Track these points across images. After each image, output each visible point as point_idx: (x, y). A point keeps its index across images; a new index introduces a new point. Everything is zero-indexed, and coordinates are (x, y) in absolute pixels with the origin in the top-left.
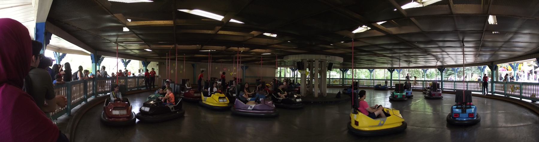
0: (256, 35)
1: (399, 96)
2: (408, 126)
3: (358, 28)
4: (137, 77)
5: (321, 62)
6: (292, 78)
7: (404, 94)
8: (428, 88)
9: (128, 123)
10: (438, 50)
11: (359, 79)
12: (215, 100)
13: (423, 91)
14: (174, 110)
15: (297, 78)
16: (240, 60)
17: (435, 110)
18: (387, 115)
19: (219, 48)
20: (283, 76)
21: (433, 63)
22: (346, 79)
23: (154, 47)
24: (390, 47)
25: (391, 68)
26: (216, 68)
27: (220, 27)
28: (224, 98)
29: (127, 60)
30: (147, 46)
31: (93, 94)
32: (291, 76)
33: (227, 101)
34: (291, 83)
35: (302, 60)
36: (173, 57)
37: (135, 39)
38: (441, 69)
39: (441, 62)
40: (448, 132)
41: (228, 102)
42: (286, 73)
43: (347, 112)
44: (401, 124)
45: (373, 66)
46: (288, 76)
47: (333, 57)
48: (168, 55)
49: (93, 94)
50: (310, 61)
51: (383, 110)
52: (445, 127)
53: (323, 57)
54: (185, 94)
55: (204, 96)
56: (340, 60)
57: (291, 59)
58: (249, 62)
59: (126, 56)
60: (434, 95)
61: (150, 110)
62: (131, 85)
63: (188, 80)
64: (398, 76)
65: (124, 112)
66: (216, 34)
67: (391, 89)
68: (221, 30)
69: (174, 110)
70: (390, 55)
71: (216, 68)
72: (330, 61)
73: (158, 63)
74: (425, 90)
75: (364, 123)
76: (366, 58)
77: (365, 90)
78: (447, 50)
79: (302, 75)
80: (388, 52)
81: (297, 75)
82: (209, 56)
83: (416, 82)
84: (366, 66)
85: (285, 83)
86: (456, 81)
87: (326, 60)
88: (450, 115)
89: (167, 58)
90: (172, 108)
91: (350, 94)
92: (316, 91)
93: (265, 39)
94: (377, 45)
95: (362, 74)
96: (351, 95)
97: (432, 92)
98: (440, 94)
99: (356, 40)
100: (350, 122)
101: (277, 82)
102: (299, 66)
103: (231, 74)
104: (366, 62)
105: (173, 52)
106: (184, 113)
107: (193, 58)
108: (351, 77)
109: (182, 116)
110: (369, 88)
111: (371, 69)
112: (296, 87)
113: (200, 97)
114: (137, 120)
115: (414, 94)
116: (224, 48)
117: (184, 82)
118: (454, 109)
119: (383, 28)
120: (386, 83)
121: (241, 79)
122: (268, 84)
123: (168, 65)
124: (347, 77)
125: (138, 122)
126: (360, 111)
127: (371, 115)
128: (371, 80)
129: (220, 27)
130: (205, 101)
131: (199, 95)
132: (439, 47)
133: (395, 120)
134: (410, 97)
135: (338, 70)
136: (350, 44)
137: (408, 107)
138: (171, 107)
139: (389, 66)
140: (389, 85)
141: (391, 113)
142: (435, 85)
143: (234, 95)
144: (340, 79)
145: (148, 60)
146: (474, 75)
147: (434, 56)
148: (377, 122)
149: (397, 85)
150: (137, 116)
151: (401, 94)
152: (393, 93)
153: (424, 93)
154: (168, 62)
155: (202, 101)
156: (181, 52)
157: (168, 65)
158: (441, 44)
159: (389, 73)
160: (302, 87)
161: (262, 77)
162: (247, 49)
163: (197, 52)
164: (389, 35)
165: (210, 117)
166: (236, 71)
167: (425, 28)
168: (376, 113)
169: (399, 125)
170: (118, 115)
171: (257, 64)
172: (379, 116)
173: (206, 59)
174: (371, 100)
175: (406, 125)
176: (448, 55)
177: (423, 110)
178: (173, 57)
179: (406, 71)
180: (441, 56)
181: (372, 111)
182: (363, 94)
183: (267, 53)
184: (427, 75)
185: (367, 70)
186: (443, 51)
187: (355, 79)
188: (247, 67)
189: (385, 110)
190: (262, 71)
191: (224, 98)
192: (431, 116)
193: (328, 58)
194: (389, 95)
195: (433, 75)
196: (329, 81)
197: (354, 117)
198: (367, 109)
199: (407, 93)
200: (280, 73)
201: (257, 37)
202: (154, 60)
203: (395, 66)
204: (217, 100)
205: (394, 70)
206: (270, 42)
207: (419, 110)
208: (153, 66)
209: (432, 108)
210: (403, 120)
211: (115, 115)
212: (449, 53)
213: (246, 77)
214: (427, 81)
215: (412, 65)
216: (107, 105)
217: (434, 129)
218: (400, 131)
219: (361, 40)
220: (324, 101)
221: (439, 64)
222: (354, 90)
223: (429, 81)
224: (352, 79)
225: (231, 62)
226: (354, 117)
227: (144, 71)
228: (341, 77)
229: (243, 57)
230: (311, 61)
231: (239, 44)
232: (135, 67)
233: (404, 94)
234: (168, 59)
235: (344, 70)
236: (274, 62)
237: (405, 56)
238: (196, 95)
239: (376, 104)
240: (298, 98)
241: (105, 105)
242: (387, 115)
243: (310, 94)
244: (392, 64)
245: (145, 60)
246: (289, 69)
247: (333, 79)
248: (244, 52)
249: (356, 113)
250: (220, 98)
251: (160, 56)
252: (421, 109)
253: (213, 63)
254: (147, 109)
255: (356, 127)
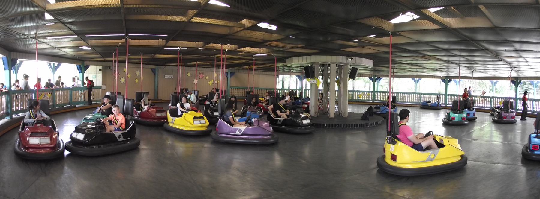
0: (248, 26)
1: (457, 119)
2: (468, 162)
3: (398, 15)
4: (70, 89)
5: (340, 66)
6: (300, 89)
7: (465, 115)
8: (498, 108)
9: (51, 158)
10: (513, 54)
11: (398, 93)
12: (187, 121)
13: (491, 111)
14: (122, 139)
15: (306, 90)
16: (225, 63)
17: (505, 138)
18: (440, 145)
19: (192, 44)
20: (286, 87)
21: (506, 73)
22: (377, 92)
23: (94, 42)
24: (446, 47)
25: (447, 77)
26: (189, 74)
27: (196, 11)
28: (202, 117)
29: (56, 64)
30: (82, 42)
31: (7, 114)
32: (298, 88)
33: (205, 122)
34: (296, 98)
35: (313, 64)
36: (122, 58)
37: (63, 31)
38: (516, 81)
39: (517, 72)
40: (522, 171)
41: (208, 123)
42: (289, 82)
43: (380, 142)
44: (460, 158)
45: (419, 74)
46: (293, 87)
47: (358, 59)
48: (115, 54)
49: (7, 114)
50: (323, 65)
51: (434, 139)
52: (520, 163)
53: (341, 59)
54: (142, 115)
55: (172, 115)
56: (370, 63)
57: (297, 62)
58: (235, 66)
59: (56, 58)
60: (505, 117)
61: (85, 138)
62: (60, 98)
63: (148, 93)
64: (456, 89)
65: (46, 140)
66: (189, 22)
67: (445, 108)
68: (197, 15)
69: (122, 139)
70: (446, 59)
71: (189, 74)
72: (354, 64)
73: (100, 67)
74: (494, 111)
75: (405, 157)
76: (410, 61)
77: (409, 109)
78: (524, 55)
79: (311, 85)
80: (443, 54)
81: (306, 86)
82: (178, 56)
83: (483, 97)
84: (409, 73)
85: (288, 98)
86: (535, 100)
87: (347, 64)
88: (527, 147)
89: (113, 59)
90: (120, 136)
91: (385, 116)
92: (333, 109)
93: (260, 33)
94: (427, 43)
95: (402, 86)
96: (386, 118)
97: (503, 114)
98: (513, 117)
99: (395, 34)
100: (384, 156)
101: (275, 96)
102: (308, 73)
103: (211, 83)
104: (409, 68)
105: (122, 50)
106: (138, 144)
107: (154, 60)
108: (385, 89)
109: (135, 148)
110: (413, 105)
111: (417, 77)
112: (304, 103)
113: (166, 118)
114: (67, 153)
115: (478, 115)
116: (199, 44)
117: (140, 96)
118: (532, 139)
119: (436, 17)
120: (439, 98)
121: (225, 91)
122: (261, 99)
123: (115, 71)
124: (380, 89)
125: (69, 155)
126: (399, 140)
127: (418, 147)
128: (416, 93)
129: (196, 11)
130: (173, 123)
131: (163, 114)
132: (516, 51)
133: (450, 154)
134: (472, 120)
135: (367, 79)
136: (385, 40)
137: (469, 134)
138: (117, 134)
139: (444, 74)
140: (442, 102)
141: (445, 142)
142: (508, 105)
143: (216, 114)
144: (369, 92)
145: (86, 63)
146: (425, 133)
147: (508, 62)
148: (426, 155)
149: (455, 102)
150: (67, 147)
151: (461, 114)
152: (448, 114)
153: (492, 115)
154: (115, 66)
155: (168, 123)
156: (135, 51)
157: (115, 71)
158: (518, 46)
159: (443, 84)
160: (312, 103)
161: (255, 88)
162: (234, 46)
163: (159, 50)
164: (445, 29)
165: (181, 147)
166: (218, 79)
167: (498, 21)
168: (424, 144)
169: (457, 159)
170: (38, 145)
171: (247, 69)
172: (428, 148)
173: (174, 60)
174: (414, 124)
175: (467, 160)
176: (527, 62)
177: (488, 139)
178: (122, 58)
179: (466, 84)
180: (516, 63)
181: (417, 142)
182: (405, 114)
183: (261, 53)
184: (496, 89)
185: (410, 79)
186: (521, 57)
187: (393, 93)
188: (232, 74)
189: (437, 139)
190: (257, 80)
191: (202, 117)
192: (501, 148)
193: (350, 61)
194: (443, 115)
195: (506, 90)
196: (353, 95)
197: (390, 149)
198: (410, 137)
199: (468, 115)
200: (283, 82)
201: (250, 28)
202: (96, 63)
203: (451, 75)
204: (191, 120)
205: (450, 81)
206: (267, 36)
207: (485, 139)
208: (94, 74)
209: (502, 136)
210: (462, 153)
211: (34, 145)
212: (528, 60)
213: (231, 87)
214: (496, 98)
215: (476, 74)
216: (22, 130)
217: (505, 166)
218: (455, 170)
219: (402, 33)
220: (343, 125)
221: (514, 74)
222: (392, 108)
223: (498, 98)
224: (389, 92)
225: (212, 66)
226: (390, 149)
227: (81, 79)
228: (372, 90)
229: (228, 59)
230: (324, 65)
231: (223, 39)
232: (69, 75)
233: (465, 115)
234: (115, 61)
235: (375, 78)
236: (271, 66)
237: (468, 60)
238: (158, 115)
239: (417, 132)
240: (306, 118)
241: (20, 130)
242: (440, 145)
243: (323, 112)
244: (448, 72)
245: (82, 63)
246: (295, 77)
247: (358, 91)
248: (230, 52)
249: (393, 142)
250: (195, 118)
251: (106, 57)
252: (487, 136)
253: (185, 67)
254: (80, 137)
255: (392, 163)
